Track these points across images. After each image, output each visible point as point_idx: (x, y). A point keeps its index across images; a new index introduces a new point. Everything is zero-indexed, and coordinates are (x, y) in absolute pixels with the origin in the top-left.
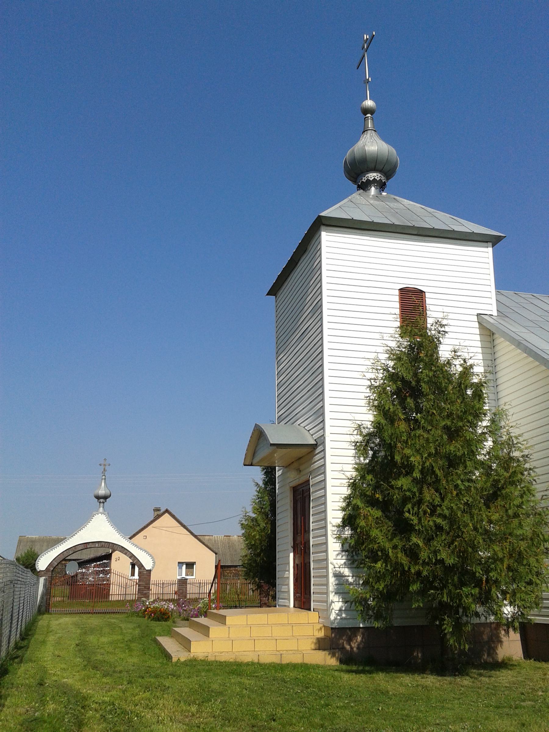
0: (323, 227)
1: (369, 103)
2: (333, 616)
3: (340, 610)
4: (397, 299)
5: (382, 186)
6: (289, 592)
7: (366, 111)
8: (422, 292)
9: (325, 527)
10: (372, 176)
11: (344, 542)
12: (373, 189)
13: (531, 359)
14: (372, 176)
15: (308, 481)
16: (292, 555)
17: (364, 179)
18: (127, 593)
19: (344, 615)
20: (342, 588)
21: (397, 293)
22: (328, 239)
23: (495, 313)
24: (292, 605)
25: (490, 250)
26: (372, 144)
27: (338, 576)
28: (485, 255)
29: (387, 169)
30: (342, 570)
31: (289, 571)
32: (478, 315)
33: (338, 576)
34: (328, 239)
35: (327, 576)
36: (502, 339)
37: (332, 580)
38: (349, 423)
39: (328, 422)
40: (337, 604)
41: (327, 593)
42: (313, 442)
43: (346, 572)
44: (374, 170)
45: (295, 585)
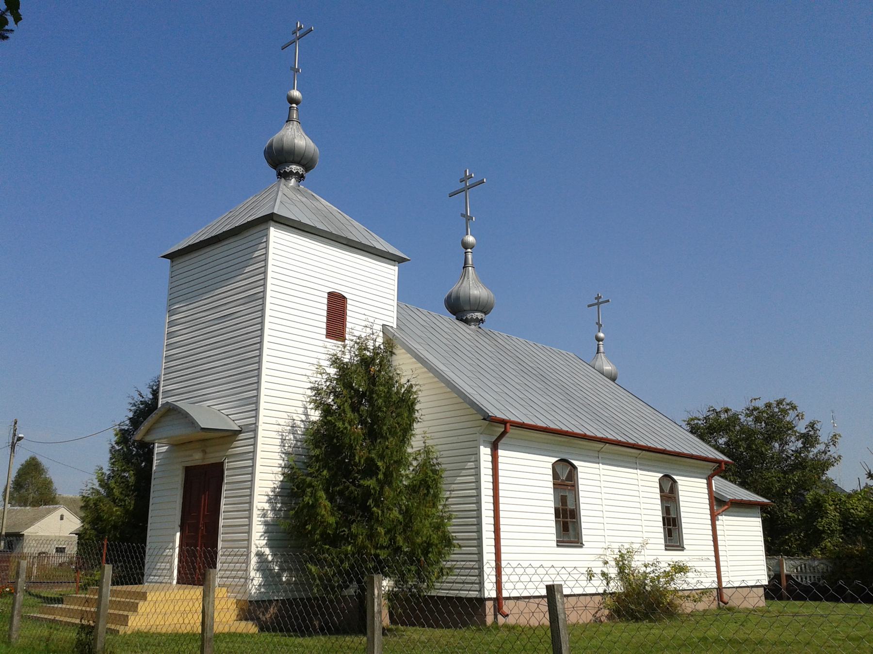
0: (272, 223)
1: (296, 93)
2: (253, 591)
3: (260, 585)
4: (326, 301)
5: (300, 178)
6: (171, 569)
7: (292, 100)
8: (344, 297)
9: (250, 510)
10: (294, 168)
11: (266, 524)
12: (293, 180)
13: (431, 375)
14: (294, 168)
15: (222, 464)
16: (178, 534)
17: (288, 169)
18: (505, 594)
19: (262, 590)
20: (263, 566)
21: (326, 295)
22: (276, 235)
23: (395, 326)
24: (175, 582)
25: (396, 268)
26: (296, 137)
27: (260, 555)
28: (391, 272)
29: (307, 163)
30: (263, 550)
31: (173, 548)
32: (383, 325)
33: (260, 555)
34: (276, 235)
35: (248, 555)
36: (403, 351)
37: (254, 560)
38: (285, 415)
39: (262, 412)
40: (256, 579)
41: (246, 570)
42: (238, 429)
43: (267, 551)
44: (298, 163)
45: (180, 561)
